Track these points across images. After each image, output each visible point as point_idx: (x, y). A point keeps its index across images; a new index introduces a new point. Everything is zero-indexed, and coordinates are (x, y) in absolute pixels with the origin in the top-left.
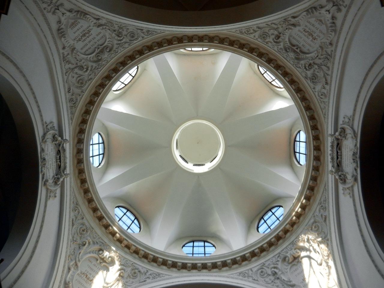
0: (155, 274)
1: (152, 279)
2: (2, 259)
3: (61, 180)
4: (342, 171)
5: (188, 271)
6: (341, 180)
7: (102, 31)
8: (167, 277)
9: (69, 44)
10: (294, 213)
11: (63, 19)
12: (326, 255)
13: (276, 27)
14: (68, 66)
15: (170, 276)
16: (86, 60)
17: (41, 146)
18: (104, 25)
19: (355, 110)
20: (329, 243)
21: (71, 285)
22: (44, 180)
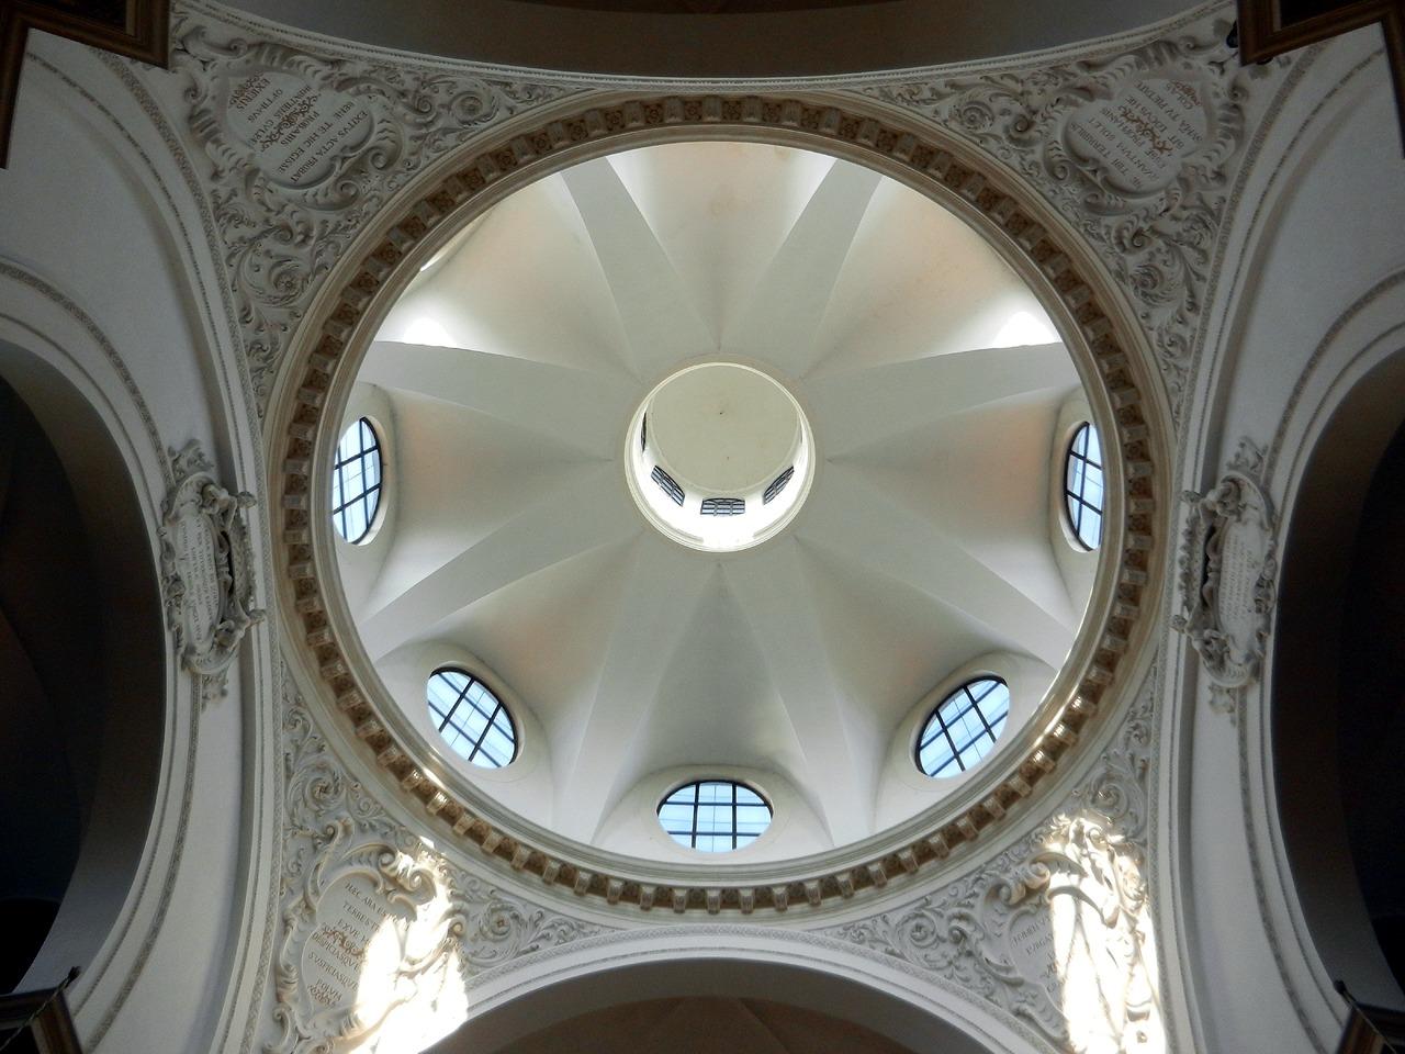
0: (566, 923)
1: (558, 943)
2: (73, 968)
3: (240, 634)
4: (1216, 629)
5: (676, 915)
6: (1210, 657)
7: (355, 101)
8: (606, 934)
9: (234, 159)
10: (1039, 741)
11: (205, 81)
12: (1132, 895)
13: (1019, 88)
14: (233, 234)
15: (617, 932)
16: (302, 203)
17: (161, 535)
18: (363, 79)
19: (1281, 433)
20: (1148, 853)
21: (294, 974)
22: (182, 650)
